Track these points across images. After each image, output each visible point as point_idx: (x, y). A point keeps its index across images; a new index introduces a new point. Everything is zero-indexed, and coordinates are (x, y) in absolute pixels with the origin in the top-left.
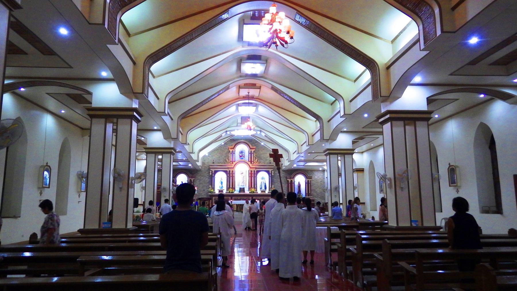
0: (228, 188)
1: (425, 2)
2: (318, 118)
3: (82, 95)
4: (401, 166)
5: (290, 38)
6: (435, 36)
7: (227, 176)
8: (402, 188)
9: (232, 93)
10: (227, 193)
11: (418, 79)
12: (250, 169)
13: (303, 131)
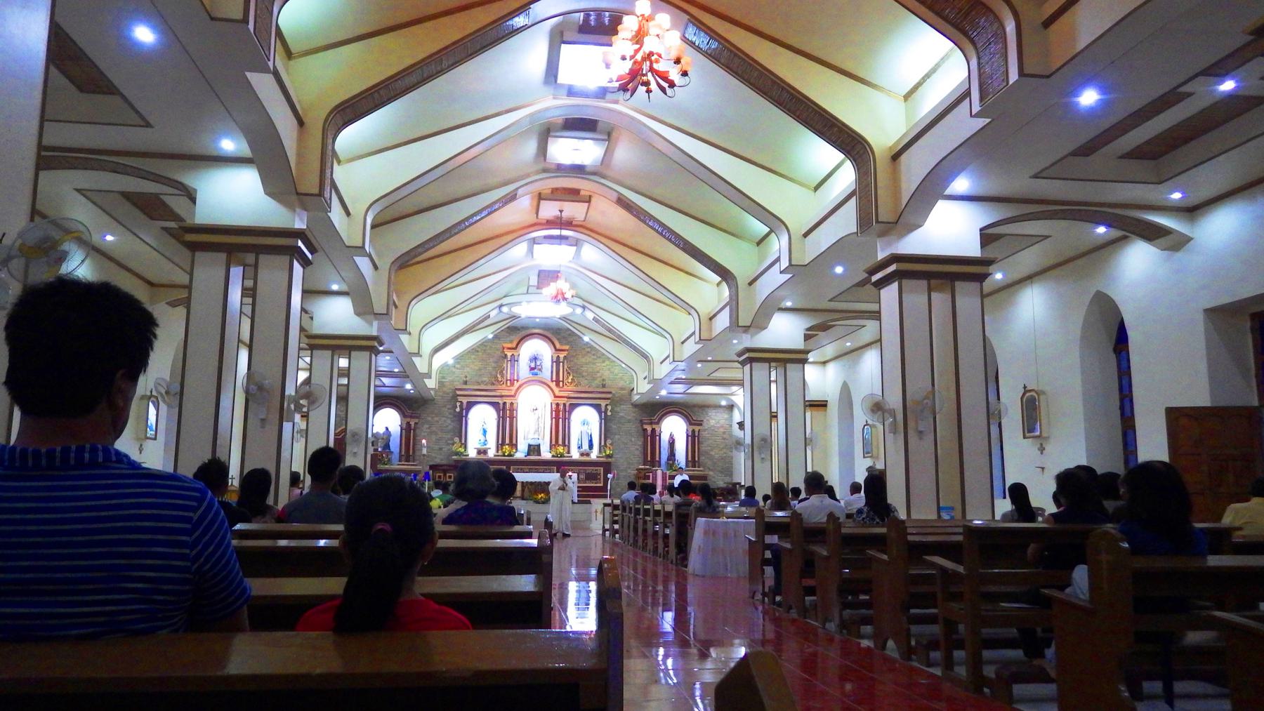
0: (500, 445)
1: (984, 5)
2: (724, 274)
3: (161, 197)
4: (918, 385)
5: (682, 75)
6: (1005, 84)
7: (499, 417)
8: (921, 432)
9: (520, 211)
10: (498, 456)
11: (961, 184)
12: (553, 398)
13: (688, 308)
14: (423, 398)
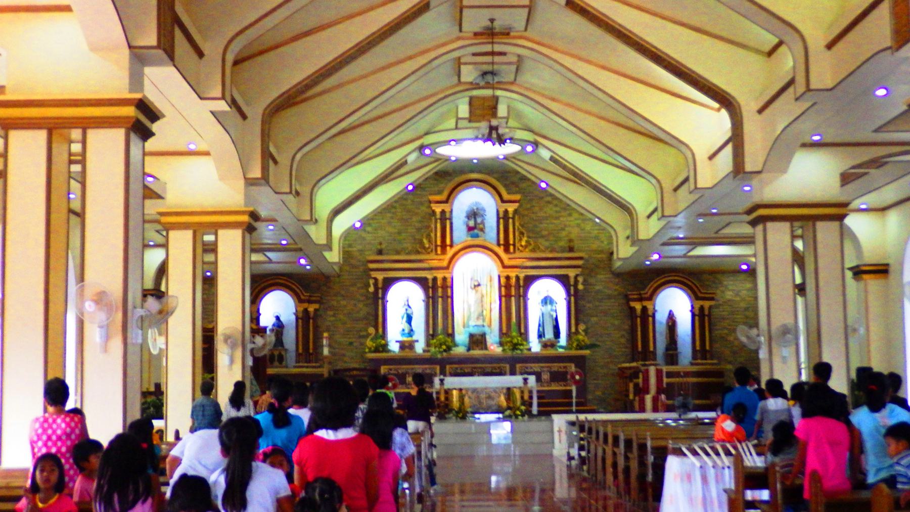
0: (431, 336)
2: (724, 100)
12: (501, 269)
14: (323, 274)
